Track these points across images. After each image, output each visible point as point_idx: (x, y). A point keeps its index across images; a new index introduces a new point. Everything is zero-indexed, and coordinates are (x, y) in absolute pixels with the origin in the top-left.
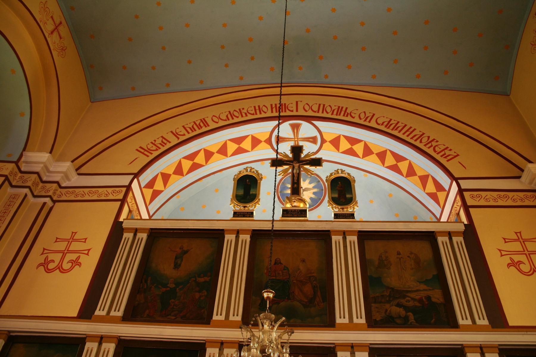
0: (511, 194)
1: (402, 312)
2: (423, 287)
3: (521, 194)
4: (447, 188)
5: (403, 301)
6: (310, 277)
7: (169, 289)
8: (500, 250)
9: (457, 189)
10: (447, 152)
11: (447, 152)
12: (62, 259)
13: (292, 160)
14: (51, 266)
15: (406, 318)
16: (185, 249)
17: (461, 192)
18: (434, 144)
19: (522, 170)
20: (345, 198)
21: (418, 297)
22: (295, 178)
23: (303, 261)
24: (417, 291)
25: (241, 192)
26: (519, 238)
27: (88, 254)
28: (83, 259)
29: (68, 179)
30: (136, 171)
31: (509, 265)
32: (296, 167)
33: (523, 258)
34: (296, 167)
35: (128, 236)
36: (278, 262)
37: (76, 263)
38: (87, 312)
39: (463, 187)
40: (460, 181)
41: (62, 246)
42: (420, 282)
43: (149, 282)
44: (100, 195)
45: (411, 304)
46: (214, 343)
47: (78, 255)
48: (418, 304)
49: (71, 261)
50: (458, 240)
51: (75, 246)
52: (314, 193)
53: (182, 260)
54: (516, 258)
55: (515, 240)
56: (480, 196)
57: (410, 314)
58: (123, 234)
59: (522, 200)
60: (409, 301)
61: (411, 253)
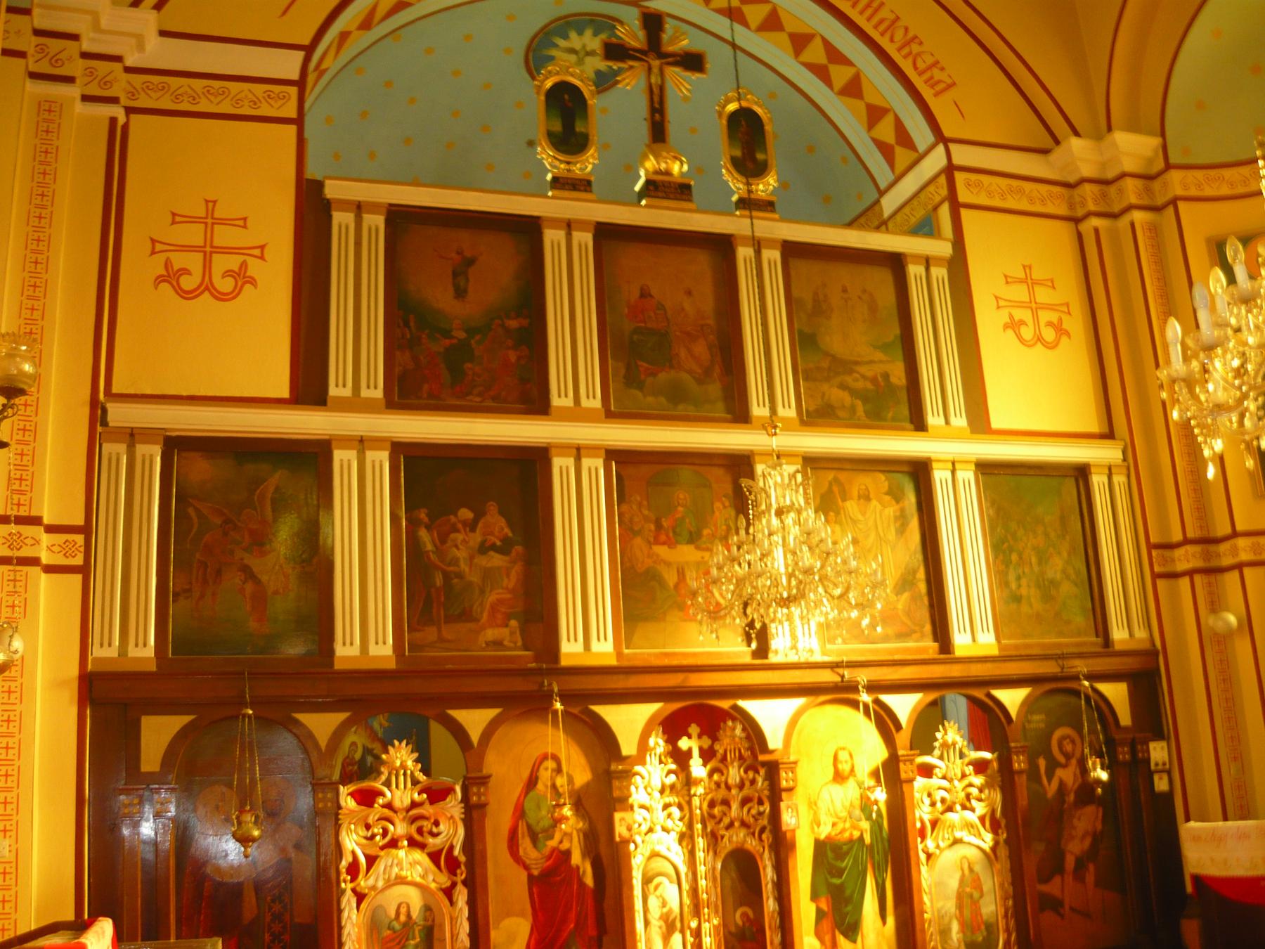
0: (1028, 186)
1: (846, 397)
2: (879, 356)
3: (1044, 188)
4: (921, 148)
5: (849, 380)
6: (702, 326)
7: (455, 341)
8: (997, 298)
9: (944, 162)
10: (937, 74)
11: (937, 74)
12: (207, 266)
13: (645, 48)
14: (188, 283)
15: (853, 410)
16: (468, 254)
17: (950, 170)
18: (915, 48)
19: (1057, 142)
20: (754, 160)
21: (870, 374)
22: (656, 99)
23: (689, 293)
24: (871, 362)
25: (557, 126)
26: (1029, 282)
27: (262, 257)
28: (254, 267)
29: (141, 47)
30: (306, 41)
31: (1006, 327)
32: (655, 70)
33: (1026, 315)
34: (655, 70)
35: (341, 219)
36: (645, 294)
37: (242, 278)
38: (309, 386)
39: (957, 160)
40: (952, 146)
41: (194, 235)
42: (876, 347)
43: (412, 324)
44: (177, 98)
45: (860, 384)
46: (565, 448)
47: (240, 258)
48: (869, 386)
49: (228, 273)
50: (939, 273)
51: (224, 236)
52: (566, 37)
53: (467, 279)
54: (1019, 314)
55: (1021, 281)
56: (979, 185)
57: (859, 403)
58: (330, 216)
59: (1043, 201)
60: (857, 380)
61: (864, 291)
